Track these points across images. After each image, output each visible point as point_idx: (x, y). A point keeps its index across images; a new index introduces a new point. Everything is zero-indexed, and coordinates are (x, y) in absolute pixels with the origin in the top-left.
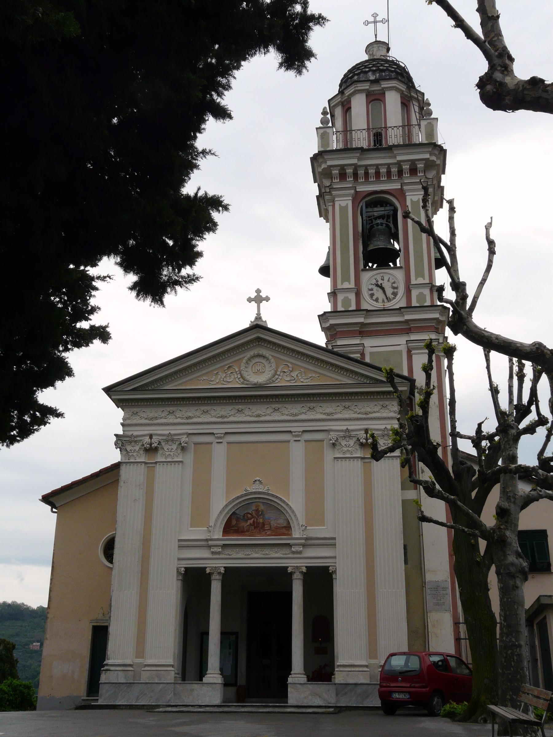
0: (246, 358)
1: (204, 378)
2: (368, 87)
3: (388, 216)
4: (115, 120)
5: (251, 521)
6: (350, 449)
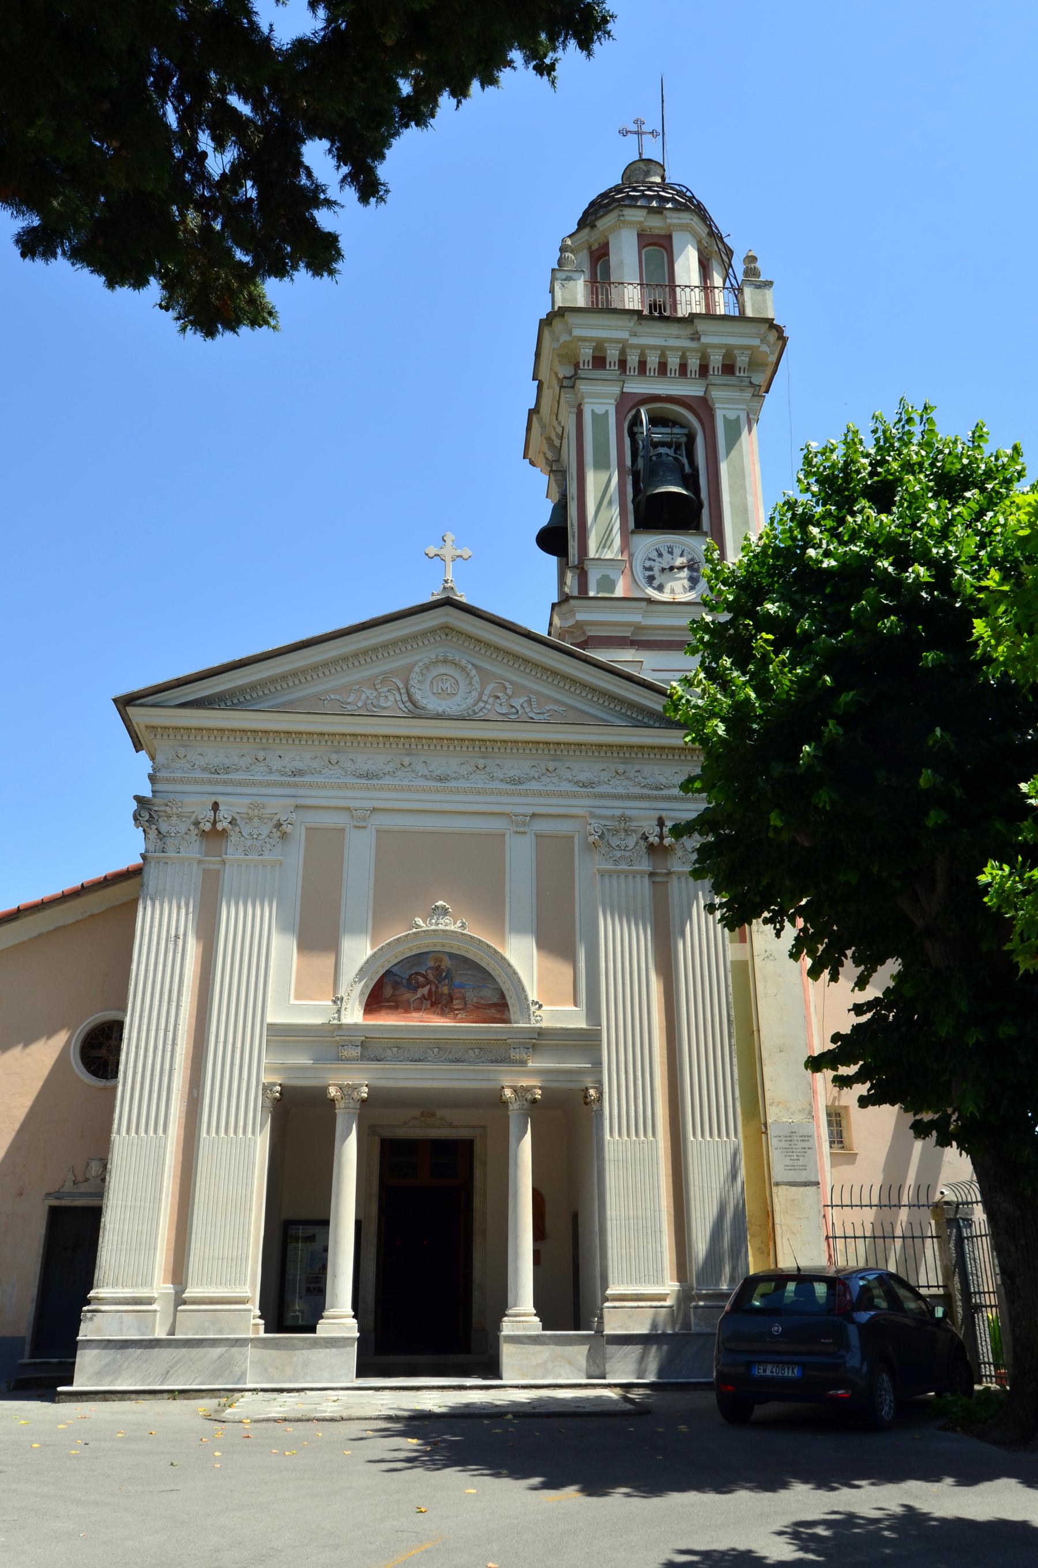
0: (421, 664)
1: (332, 696)
2: (642, 219)
3: (678, 447)
5: (425, 990)
6: (627, 854)
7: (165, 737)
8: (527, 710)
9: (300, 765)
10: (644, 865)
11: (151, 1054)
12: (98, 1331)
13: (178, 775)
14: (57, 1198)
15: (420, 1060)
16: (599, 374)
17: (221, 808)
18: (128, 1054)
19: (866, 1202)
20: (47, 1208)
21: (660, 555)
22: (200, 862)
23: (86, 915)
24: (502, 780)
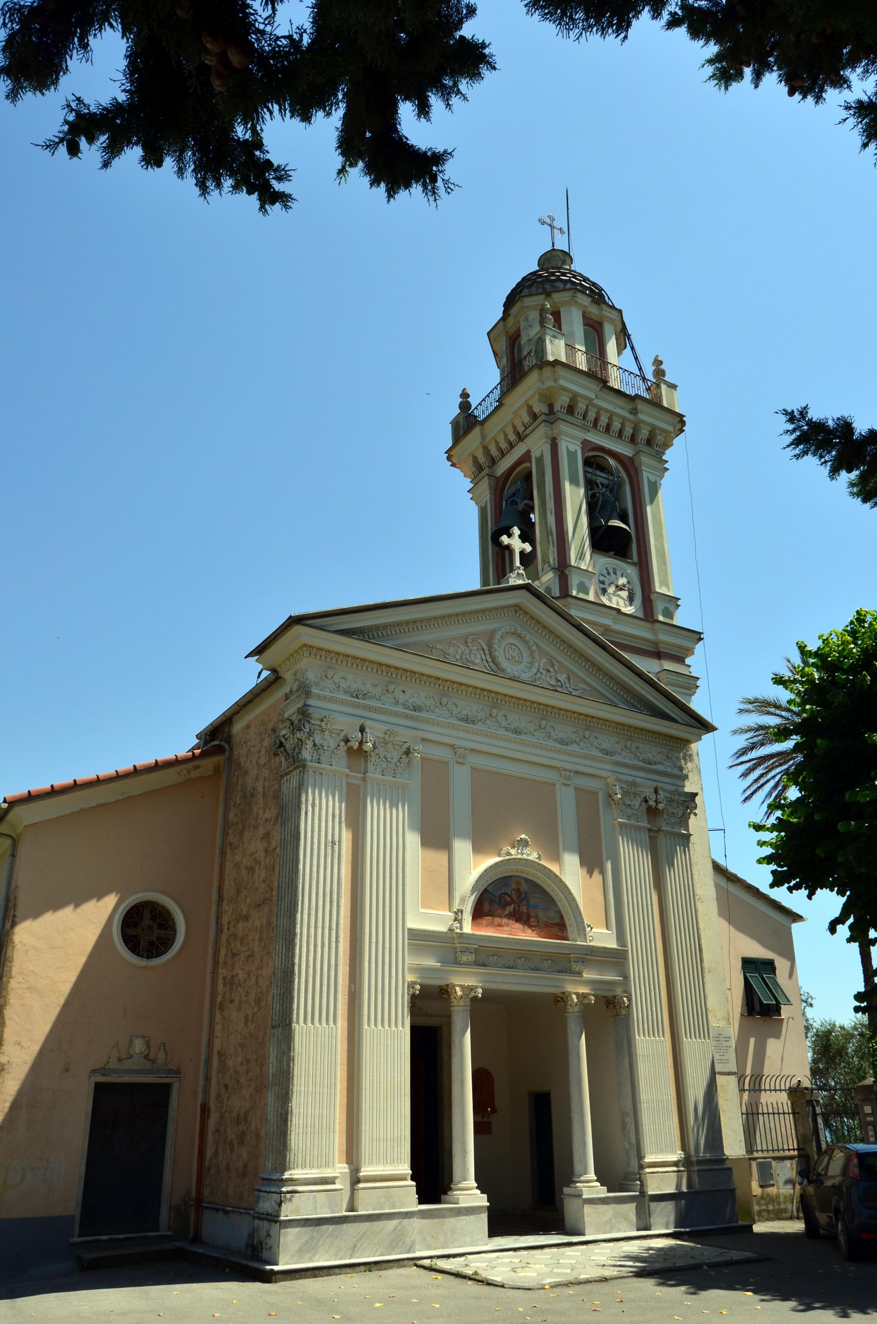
2: (587, 304)
4: (368, 135)
7: (318, 657)
8: (568, 685)
9: (418, 702)
10: (644, 823)
11: (319, 949)
12: (297, 1210)
13: (327, 693)
14: (104, 1075)
15: (512, 968)
16: (569, 418)
17: (367, 730)
18: (301, 948)
19: (772, 1088)
20: (93, 1085)
21: (609, 573)
22: (347, 776)
23: (125, 796)
24: (555, 740)
